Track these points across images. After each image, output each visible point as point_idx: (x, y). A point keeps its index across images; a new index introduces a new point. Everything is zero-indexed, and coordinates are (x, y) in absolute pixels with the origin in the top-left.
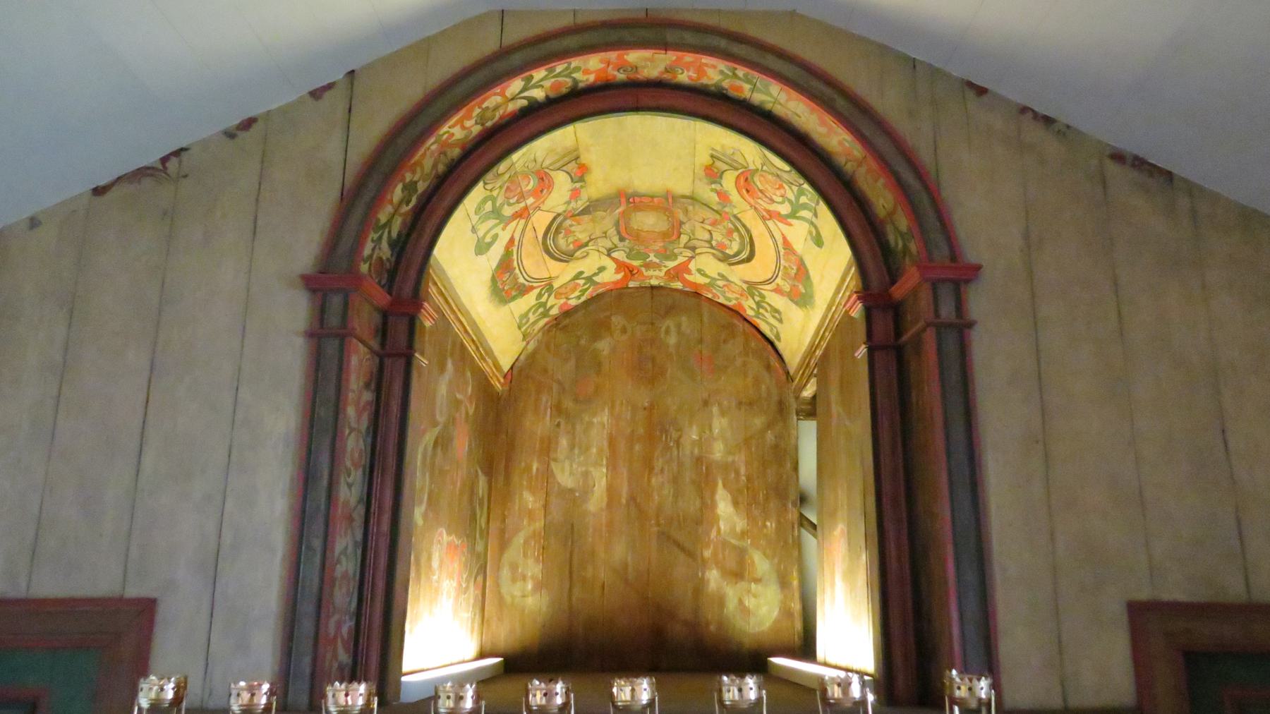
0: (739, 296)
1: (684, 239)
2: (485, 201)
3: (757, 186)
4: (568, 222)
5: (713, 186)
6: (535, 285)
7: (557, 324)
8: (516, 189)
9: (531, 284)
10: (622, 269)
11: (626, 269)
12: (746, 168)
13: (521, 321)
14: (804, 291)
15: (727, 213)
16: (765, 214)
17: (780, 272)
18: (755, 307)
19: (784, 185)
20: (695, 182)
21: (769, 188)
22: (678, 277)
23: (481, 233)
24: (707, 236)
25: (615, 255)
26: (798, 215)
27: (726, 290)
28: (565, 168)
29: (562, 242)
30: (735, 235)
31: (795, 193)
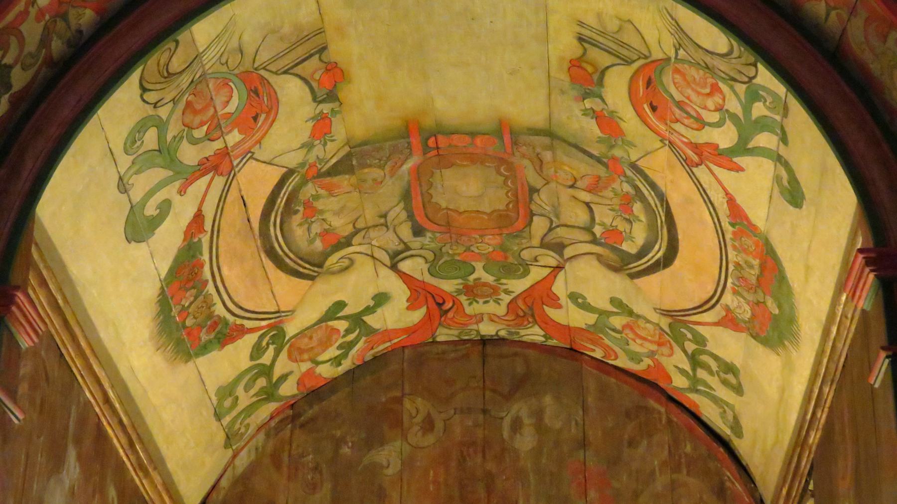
0: (654, 347)
1: (539, 226)
2: (141, 127)
3: (672, 96)
4: (310, 190)
5: (588, 104)
6: (249, 324)
7: (294, 418)
8: (205, 108)
9: (239, 321)
10: (422, 298)
11: (430, 300)
12: (646, 57)
13: (220, 400)
14: (776, 311)
15: (614, 159)
16: (690, 153)
17: (730, 281)
18: (687, 367)
19: (721, 85)
20: (553, 97)
21: (694, 97)
22: (533, 316)
23: (137, 195)
24: (582, 217)
25: (405, 266)
26: (750, 146)
27: (631, 335)
28: (295, 70)
29: (299, 233)
30: (637, 207)
31: (742, 97)
